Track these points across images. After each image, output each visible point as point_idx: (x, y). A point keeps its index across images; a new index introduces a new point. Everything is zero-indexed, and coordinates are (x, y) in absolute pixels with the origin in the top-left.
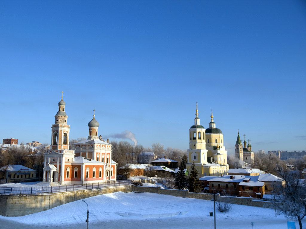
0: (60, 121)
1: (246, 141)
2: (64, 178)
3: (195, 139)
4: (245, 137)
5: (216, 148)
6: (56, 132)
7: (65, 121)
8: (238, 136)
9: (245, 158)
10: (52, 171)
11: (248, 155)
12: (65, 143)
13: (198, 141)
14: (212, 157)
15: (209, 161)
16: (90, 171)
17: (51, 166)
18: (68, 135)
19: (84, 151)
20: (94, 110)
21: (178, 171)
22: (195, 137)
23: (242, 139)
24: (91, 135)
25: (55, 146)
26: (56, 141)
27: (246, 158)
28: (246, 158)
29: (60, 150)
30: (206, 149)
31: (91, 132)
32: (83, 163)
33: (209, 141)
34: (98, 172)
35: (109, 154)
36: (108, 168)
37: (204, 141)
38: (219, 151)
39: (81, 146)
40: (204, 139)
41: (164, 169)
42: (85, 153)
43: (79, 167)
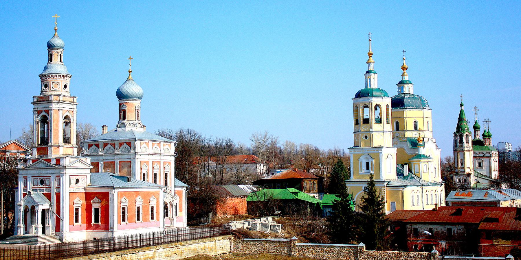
0: (52, 85)
1: (480, 124)
2: (25, 231)
3: (366, 121)
4: (476, 114)
5: (415, 144)
6: (44, 113)
7: (65, 87)
8: (461, 110)
9: (477, 164)
10: (40, 208)
11: (483, 157)
12: (67, 141)
13: (376, 127)
14: (406, 164)
15: (400, 174)
16: (129, 206)
17: (37, 197)
18: (74, 121)
19: (110, 159)
20: (130, 59)
21: (335, 200)
22: (366, 117)
23: (470, 120)
24: (124, 119)
25: (44, 148)
26: (46, 136)
27: (480, 164)
28: (480, 164)
29: (57, 156)
30: (394, 144)
31: (124, 112)
32: (113, 188)
33: (398, 127)
34: (148, 207)
35: (170, 163)
36: (168, 200)
37: (388, 127)
38: (422, 151)
39: (101, 145)
40: (388, 123)
41: (296, 197)
42: (113, 163)
43: (104, 197)
